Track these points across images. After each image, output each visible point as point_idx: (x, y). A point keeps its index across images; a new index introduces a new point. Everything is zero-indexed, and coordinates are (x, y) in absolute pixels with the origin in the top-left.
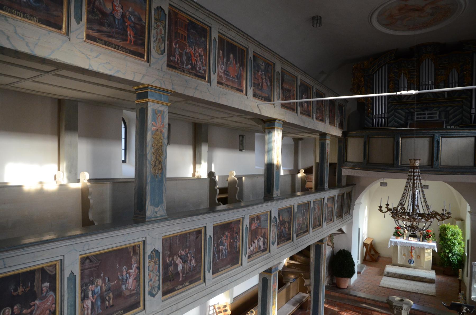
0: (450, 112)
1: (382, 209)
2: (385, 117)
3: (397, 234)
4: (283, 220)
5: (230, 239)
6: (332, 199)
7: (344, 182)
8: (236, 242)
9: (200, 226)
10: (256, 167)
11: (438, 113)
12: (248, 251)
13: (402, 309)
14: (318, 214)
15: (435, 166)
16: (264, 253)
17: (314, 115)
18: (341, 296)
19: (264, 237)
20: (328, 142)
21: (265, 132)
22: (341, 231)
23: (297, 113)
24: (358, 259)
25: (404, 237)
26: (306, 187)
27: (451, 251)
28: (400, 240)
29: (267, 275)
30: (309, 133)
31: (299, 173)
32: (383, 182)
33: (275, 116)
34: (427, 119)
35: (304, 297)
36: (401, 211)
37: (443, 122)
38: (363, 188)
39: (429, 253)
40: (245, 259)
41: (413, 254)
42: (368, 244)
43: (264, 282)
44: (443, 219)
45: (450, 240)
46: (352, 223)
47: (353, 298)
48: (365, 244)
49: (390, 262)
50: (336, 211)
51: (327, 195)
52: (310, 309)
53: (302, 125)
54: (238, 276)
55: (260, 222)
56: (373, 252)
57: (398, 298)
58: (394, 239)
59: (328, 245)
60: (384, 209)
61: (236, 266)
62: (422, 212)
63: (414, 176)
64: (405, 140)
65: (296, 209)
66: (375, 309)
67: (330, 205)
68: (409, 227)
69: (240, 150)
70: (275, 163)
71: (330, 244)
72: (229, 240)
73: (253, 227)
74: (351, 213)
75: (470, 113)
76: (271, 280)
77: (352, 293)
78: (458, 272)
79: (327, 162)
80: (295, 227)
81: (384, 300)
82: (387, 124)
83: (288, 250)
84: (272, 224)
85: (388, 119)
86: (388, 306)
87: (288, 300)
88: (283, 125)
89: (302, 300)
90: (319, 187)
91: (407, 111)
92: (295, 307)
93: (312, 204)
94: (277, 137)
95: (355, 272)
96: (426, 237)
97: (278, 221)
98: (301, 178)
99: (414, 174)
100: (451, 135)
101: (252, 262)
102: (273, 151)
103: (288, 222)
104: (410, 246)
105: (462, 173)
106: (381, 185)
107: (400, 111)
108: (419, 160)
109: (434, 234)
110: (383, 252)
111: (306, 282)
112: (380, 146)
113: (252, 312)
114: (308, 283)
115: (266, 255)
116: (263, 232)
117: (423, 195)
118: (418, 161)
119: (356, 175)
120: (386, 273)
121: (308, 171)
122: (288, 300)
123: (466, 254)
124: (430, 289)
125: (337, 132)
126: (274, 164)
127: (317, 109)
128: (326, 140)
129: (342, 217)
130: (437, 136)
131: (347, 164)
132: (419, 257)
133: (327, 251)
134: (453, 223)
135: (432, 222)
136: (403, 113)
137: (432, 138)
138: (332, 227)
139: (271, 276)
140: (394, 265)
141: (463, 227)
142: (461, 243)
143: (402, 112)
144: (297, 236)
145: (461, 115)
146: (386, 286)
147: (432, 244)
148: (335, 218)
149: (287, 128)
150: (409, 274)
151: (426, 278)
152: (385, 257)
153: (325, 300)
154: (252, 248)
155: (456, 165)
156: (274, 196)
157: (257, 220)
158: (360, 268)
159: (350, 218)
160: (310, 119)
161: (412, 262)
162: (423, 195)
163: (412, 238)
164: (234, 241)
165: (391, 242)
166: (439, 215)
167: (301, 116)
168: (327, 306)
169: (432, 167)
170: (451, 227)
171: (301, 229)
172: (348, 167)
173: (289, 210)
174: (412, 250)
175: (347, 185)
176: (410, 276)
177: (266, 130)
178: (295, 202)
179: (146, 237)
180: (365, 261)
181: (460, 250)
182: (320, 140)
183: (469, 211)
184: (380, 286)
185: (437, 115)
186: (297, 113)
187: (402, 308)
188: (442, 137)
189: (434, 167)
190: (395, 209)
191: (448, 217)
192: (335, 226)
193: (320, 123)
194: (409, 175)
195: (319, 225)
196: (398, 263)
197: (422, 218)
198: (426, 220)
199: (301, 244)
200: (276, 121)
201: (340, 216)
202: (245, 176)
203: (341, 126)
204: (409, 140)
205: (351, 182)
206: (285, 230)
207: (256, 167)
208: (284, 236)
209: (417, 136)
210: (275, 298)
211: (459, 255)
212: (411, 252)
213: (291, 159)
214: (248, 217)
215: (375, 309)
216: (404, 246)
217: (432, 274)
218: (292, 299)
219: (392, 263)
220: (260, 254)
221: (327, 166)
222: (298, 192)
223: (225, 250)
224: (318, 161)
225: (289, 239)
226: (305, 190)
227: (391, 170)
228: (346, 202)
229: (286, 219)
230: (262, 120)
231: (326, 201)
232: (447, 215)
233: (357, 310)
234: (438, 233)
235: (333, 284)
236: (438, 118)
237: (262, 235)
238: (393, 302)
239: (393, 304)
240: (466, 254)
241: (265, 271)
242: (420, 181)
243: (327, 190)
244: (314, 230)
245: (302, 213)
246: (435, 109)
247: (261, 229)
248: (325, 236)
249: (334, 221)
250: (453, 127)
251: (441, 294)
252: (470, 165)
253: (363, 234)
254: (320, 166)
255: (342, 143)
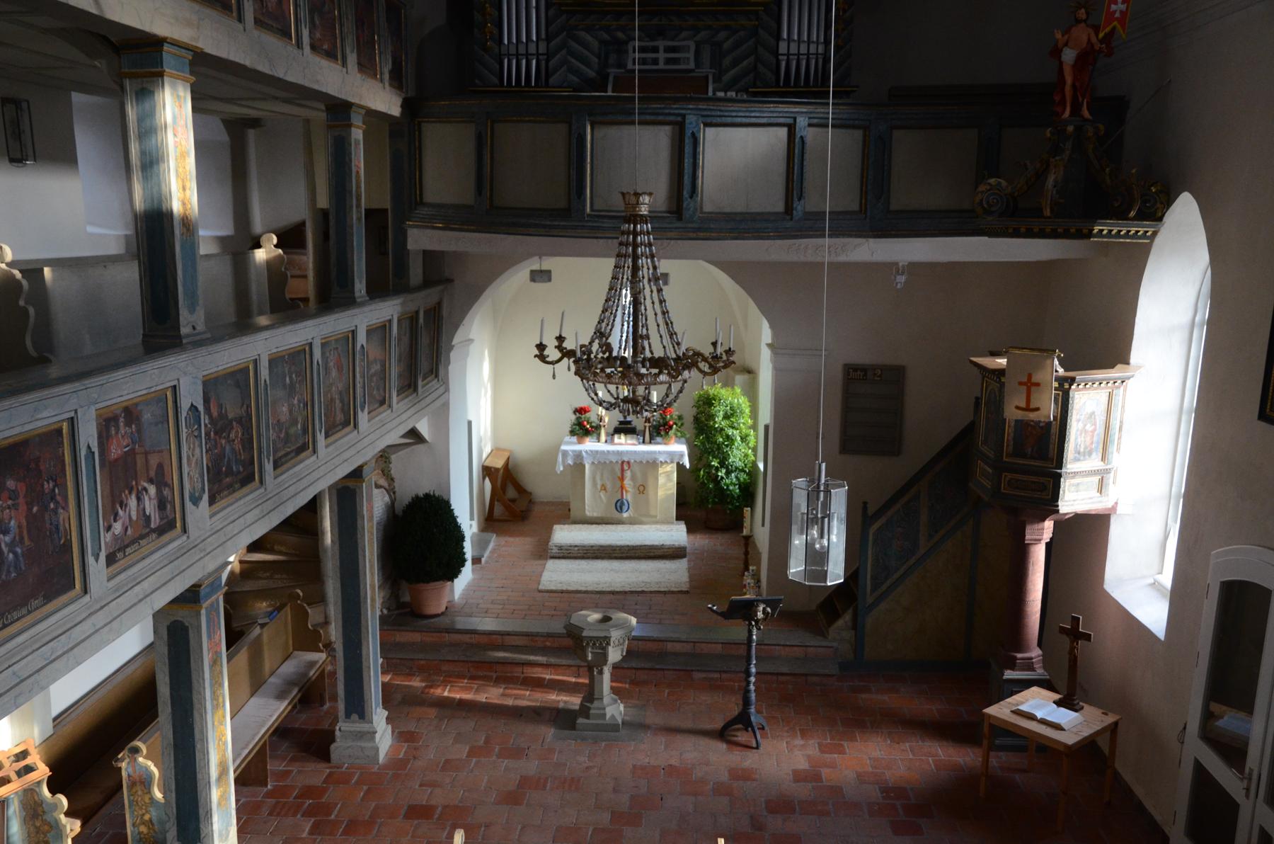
0: (726, 46)
1: (546, 353)
2: (538, 54)
3: (583, 428)
4: (222, 416)
5: (29, 506)
6: (380, 332)
7: (416, 273)
8: (55, 511)
9: (55, 419)
10: (90, 229)
11: (692, 45)
12: (106, 538)
13: (608, 644)
14: (341, 386)
15: (686, 214)
16: (166, 537)
17: (305, 33)
18: (429, 638)
19: (161, 481)
20: (357, 134)
21: (122, 88)
22: (414, 434)
23: (240, 19)
24: (472, 519)
25: (599, 435)
26: (288, 296)
27: (722, 464)
28: (589, 445)
29: (182, 614)
30: (287, 101)
31: (259, 247)
32: (536, 267)
33: (159, 28)
34: (661, 66)
35: (312, 664)
36: (600, 355)
37: (707, 77)
38: (473, 295)
39: (668, 474)
40: (97, 569)
41: (627, 482)
42: (497, 470)
43: (176, 636)
44: (715, 370)
45: (722, 429)
46: (446, 406)
47: (466, 638)
48: (487, 471)
49: (565, 513)
50: (394, 371)
51: (368, 317)
52: (334, 698)
53: (263, 68)
54: (77, 634)
55: (139, 431)
56: (511, 493)
57: (595, 616)
58: (571, 446)
59: (378, 486)
60: (553, 354)
61: (64, 598)
62: (659, 353)
63: (635, 246)
64: (602, 132)
65: (264, 373)
66: (532, 658)
67: (375, 352)
68: (626, 400)
69: (12, 160)
70: (176, 207)
71: (382, 482)
72: (23, 508)
73: (115, 452)
74: (441, 372)
75: (776, 54)
76: (199, 627)
77: (461, 623)
78: (742, 517)
79: (359, 206)
80: (267, 436)
81: (557, 627)
82: (545, 75)
83: (250, 517)
84: (184, 432)
85: (547, 61)
86: (568, 642)
87: (256, 684)
88: (192, 64)
89: (305, 674)
90: (332, 294)
91: (606, 36)
92: (286, 703)
93: (264, 373)
94: (174, 112)
95: (465, 560)
96: (659, 430)
97: (204, 419)
98: (270, 264)
99: (635, 238)
100: (729, 120)
101: (123, 576)
102: (162, 167)
103: (239, 420)
104: (619, 459)
105: (758, 234)
106: (533, 280)
107: (583, 34)
108: (650, 194)
109: (680, 418)
110: (541, 489)
111: (314, 615)
112: (528, 149)
113: (136, 751)
114: (320, 619)
115: (176, 543)
116: (154, 461)
117: (662, 301)
118: (647, 199)
119: (452, 248)
120: (555, 550)
121: (290, 239)
122: (256, 684)
123: (761, 466)
124: (673, 574)
125: (386, 102)
126: (170, 214)
127: (311, 12)
128: (350, 126)
129: (416, 390)
130: (691, 119)
131: (424, 211)
132: (642, 489)
133: (375, 505)
134: (728, 383)
135: (685, 381)
136: (595, 44)
137: (680, 126)
138: (388, 426)
139: (198, 614)
140: (575, 522)
141: (751, 392)
142: (747, 436)
143: (589, 38)
144: (276, 465)
145: (752, 59)
146: (559, 587)
147: (676, 449)
148: (394, 394)
149: (213, 82)
150: (608, 543)
151: (662, 547)
152: (548, 503)
153: (380, 661)
154: (118, 527)
155: (739, 210)
156: (184, 330)
157: (128, 424)
158: (480, 544)
159: (442, 390)
160: (292, 50)
161: (625, 508)
162: (662, 301)
163: (623, 436)
164: (44, 508)
165: (565, 453)
166: (705, 359)
167: (256, 33)
168: (387, 678)
169: (680, 218)
170: (724, 393)
171: (287, 440)
172: (428, 223)
173: (240, 378)
174: (623, 470)
175: (427, 283)
176: (621, 548)
177: (127, 83)
178: (265, 345)
179: (76, 411)
180: (490, 522)
181: (746, 455)
182: (329, 127)
183: (768, 345)
184: (540, 591)
185: (691, 55)
186: (240, 19)
187: (607, 640)
188: (706, 125)
189: (685, 219)
190: (586, 350)
191: (728, 364)
192: (398, 420)
193: (325, 63)
194: (621, 244)
195: (346, 423)
196: (588, 513)
197: (661, 372)
198: (673, 377)
199: (292, 490)
200: (166, 47)
201: (409, 386)
202: (55, 263)
203: (397, 80)
204: (613, 132)
205: (438, 272)
206: (233, 449)
207: (90, 229)
208: (230, 472)
209: (643, 117)
210: (221, 685)
211: (743, 470)
212: (622, 479)
213: (224, 196)
214: (92, 413)
215: (532, 658)
216: (602, 463)
217: (676, 534)
218: (272, 680)
219: (569, 517)
220: (147, 545)
221: (359, 219)
222: (261, 313)
223: (11, 546)
224: (323, 202)
225: (247, 479)
226: (287, 308)
227: (565, 227)
228: (424, 340)
229: (232, 412)
230: (105, 38)
231: (362, 339)
232: (724, 357)
233: (481, 674)
234: (689, 414)
235: (401, 605)
236: (692, 65)
237: (152, 474)
238: (582, 629)
239: (584, 634)
240: (761, 466)
241: (175, 601)
242: (653, 262)
243: (362, 304)
244: (331, 439)
245: (284, 385)
246: (684, 34)
247: (146, 453)
248: (368, 457)
249: (390, 406)
250: (732, 94)
251: (701, 586)
252: (769, 209)
253: (480, 441)
254: (330, 223)
255: (401, 138)
